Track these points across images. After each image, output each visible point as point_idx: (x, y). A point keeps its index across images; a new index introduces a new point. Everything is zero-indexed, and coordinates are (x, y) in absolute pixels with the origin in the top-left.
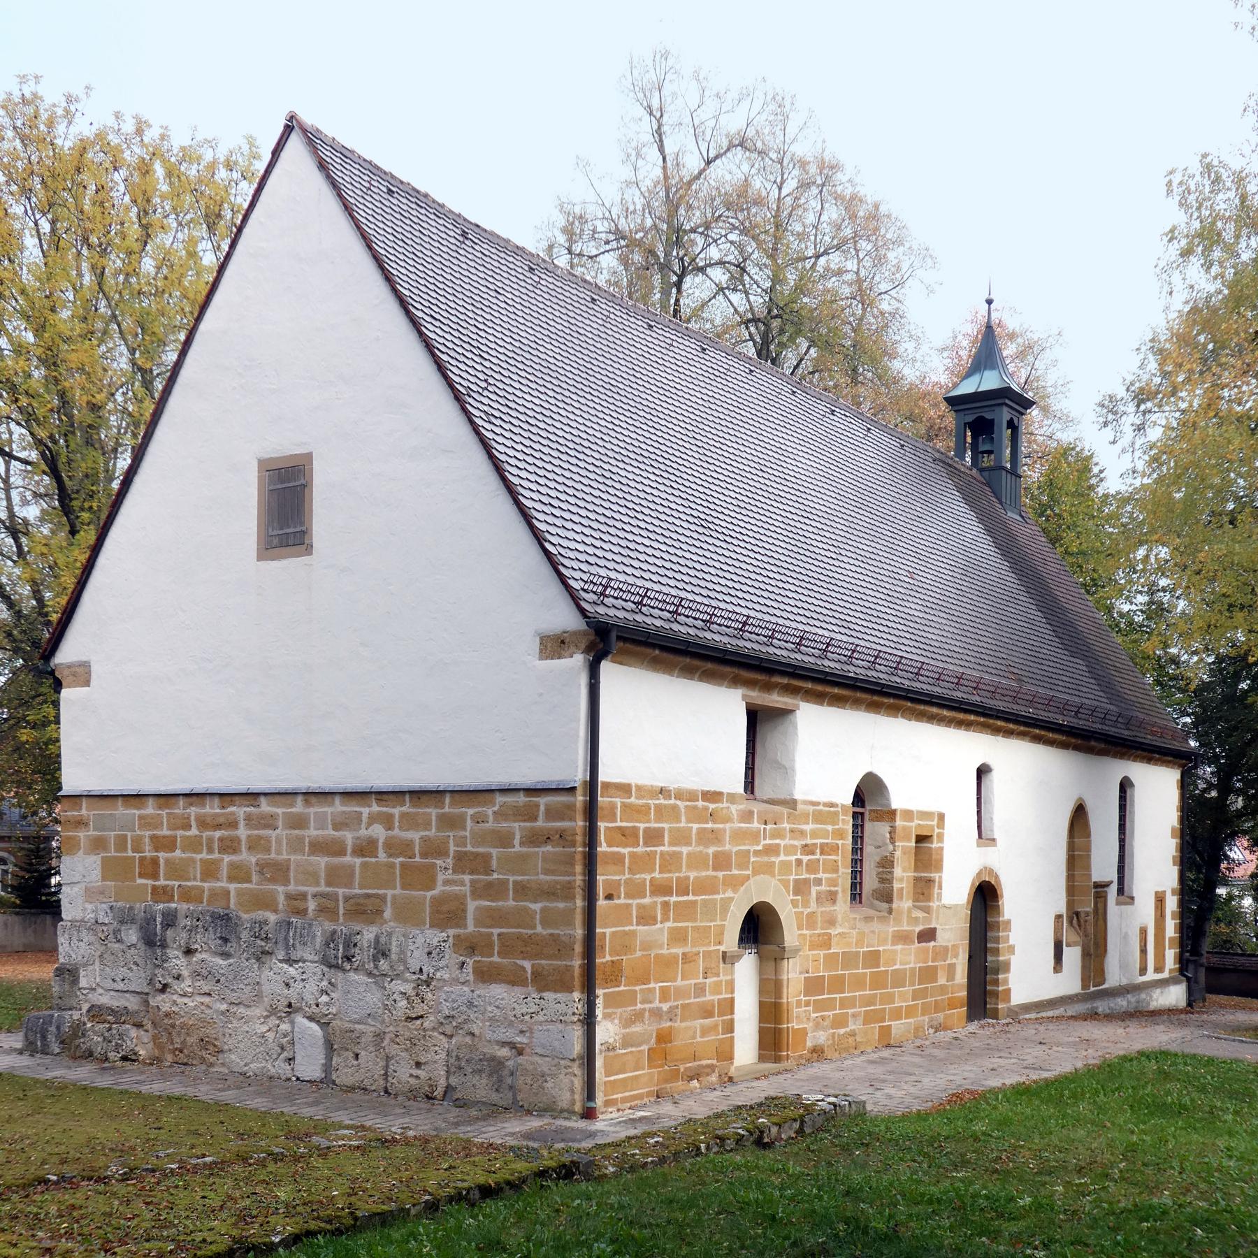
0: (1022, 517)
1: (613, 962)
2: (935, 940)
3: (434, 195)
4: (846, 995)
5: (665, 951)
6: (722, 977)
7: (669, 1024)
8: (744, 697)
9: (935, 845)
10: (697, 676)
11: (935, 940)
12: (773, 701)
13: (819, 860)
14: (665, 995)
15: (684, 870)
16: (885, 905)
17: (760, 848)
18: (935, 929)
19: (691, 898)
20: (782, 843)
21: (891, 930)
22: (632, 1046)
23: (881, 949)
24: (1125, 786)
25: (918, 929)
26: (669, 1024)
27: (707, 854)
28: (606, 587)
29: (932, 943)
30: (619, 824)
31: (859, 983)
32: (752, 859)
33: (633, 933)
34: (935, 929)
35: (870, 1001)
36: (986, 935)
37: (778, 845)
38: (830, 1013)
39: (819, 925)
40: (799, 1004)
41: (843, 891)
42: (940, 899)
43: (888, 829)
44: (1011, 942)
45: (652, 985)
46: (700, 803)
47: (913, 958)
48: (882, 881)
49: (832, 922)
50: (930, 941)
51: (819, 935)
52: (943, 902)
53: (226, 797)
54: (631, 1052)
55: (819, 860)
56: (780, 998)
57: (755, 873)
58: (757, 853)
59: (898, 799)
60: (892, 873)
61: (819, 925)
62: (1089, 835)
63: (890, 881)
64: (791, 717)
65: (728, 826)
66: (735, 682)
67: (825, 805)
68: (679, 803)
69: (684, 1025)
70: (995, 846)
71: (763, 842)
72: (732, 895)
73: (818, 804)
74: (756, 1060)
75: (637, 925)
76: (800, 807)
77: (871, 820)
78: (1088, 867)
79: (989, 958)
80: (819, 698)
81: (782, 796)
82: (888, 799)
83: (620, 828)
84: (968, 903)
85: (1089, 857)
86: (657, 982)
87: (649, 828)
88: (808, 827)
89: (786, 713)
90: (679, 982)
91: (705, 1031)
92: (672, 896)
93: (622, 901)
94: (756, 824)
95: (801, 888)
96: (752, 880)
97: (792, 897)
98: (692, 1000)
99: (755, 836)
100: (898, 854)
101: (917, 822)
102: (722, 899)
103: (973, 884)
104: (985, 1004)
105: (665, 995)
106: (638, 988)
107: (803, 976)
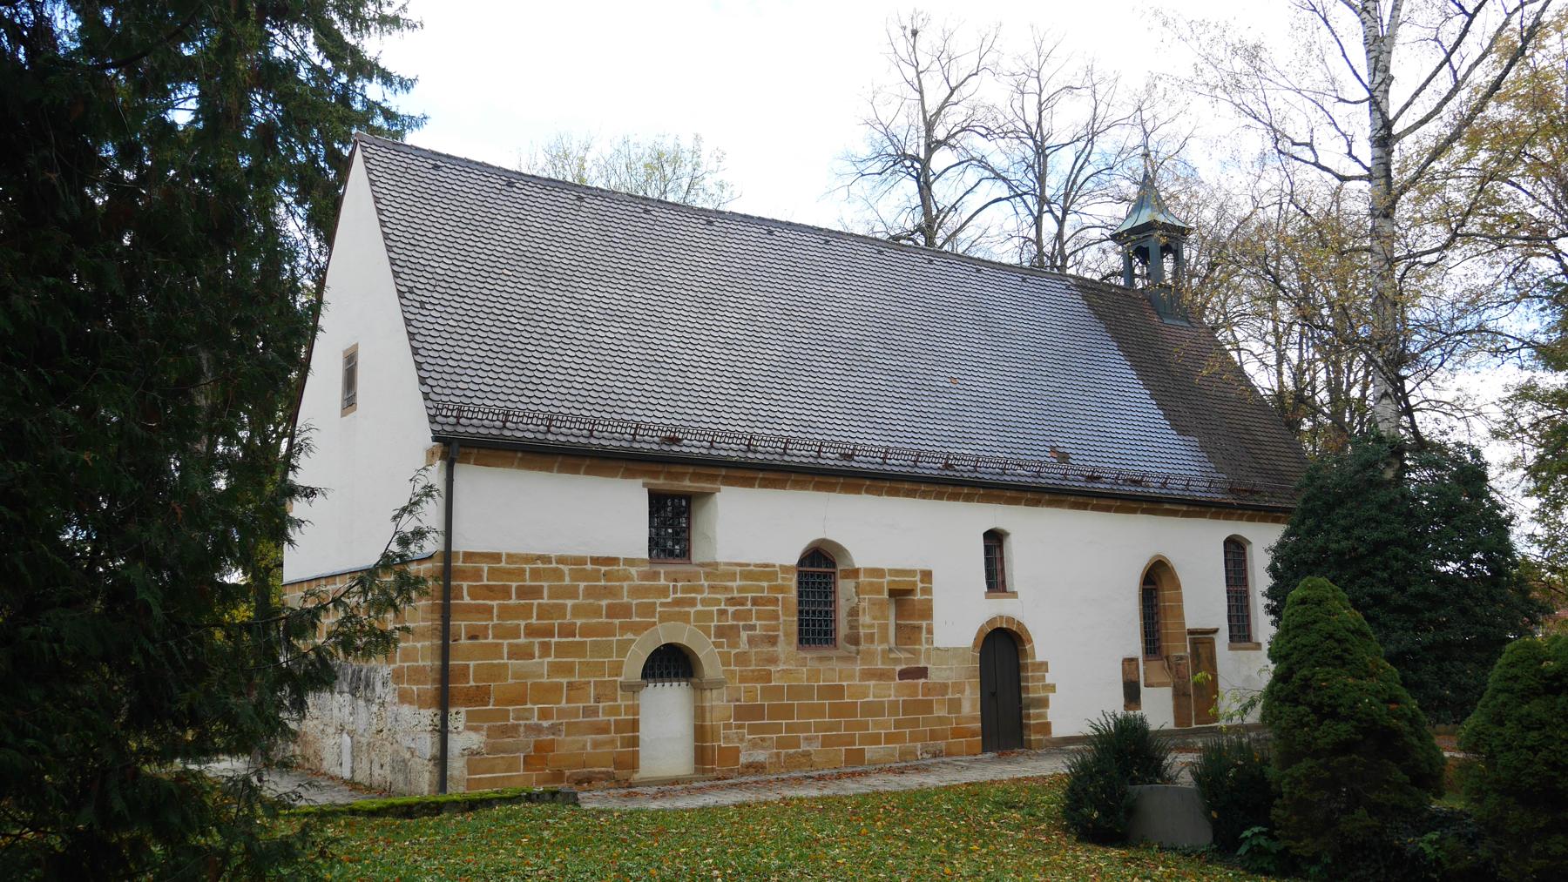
0: (1189, 322)
1: (478, 687)
2: (926, 677)
3: (469, 158)
4: (766, 721)
5: (545, 680)
6: (619, 702)
7: (552, 737)
8: (644, 485)
9: (918, 597)
10: (582, 471)
11: (926, 677)
12: (685, 486)
13: (751, 610)
14: (544, 714)
15: (568, 617)
16: (853, 648)
17: (669, 600)
18: (926, 668)
19: (577, 639)
20: (699, 597)
21: (858, 668)
22: (502, 752)
23: (845, 683)
24: (994, 540)
25: (898, 668)
26: (552, 737)
27: (601, 606)
28: (458, 418)
29: (923, 680)
30: (485, 582)
31: (817, 711)
32: (658, 609)
33: (505, 665)
34: (926, 668)
35: (830, 727)
36: (1019, 675)
37: (695, 598)
38: (774, 736)
39: (754, 662)
40: (727, 727)
41: (786, 635)
42: (930, 641)
43: (853, 584)
44: (1049, 679)
45: (529, 706)
46: (589, 567)
47: (892, 692)
48: (851, 627)
49: (773, 660)
50: (921, 678)
51: (753, 671)
52: (935, 645)
53: (309, 581)
54: (502, 757)
55: (751, 610)
56: (704, 721)
57: (662, 620)
58: (662, 605)
59: (861, 557)
60: (857, 621)
61: (754, 662)
62: (1178, 587)
63: (857, 628)
64: (713, 498)
65: (625, 584)
66: (630, 474)
67: (756, 565)
68: (561, 566)
69: (569, 739)
70: (1017, 597)
71: (672, 596)
72: (632, 637)
73: (748, 565)
74: (692, 772)
75: (508, 659)
76: (722, 568)
77: (842, 578)
78: (1181, 615)
79: (1023, 696)
80: (731, 481)
81: (707, 560)
82: (851, 560)
83: (487, 586)
84: (975, 645)
85: (1180, 608)
86: (535, 703)
87: (523, 586)
88: (734, 584)
89: (706, 495)
90: (563, 704)
91: (596, 745)
92: (553, 636)
93: (490, 640)
94: (663, 582)
95: (726, 633)
96: (659, 626)
97: (713, 639)
98: (581, 719)
99: (664, 592)
100: (864, 604)
101: (888, 578)
102: (618, 640)
103: (981, 630)
104: (1022, 737)
105: (544, 714)
106: (510, 708)
107: (732, 704)
